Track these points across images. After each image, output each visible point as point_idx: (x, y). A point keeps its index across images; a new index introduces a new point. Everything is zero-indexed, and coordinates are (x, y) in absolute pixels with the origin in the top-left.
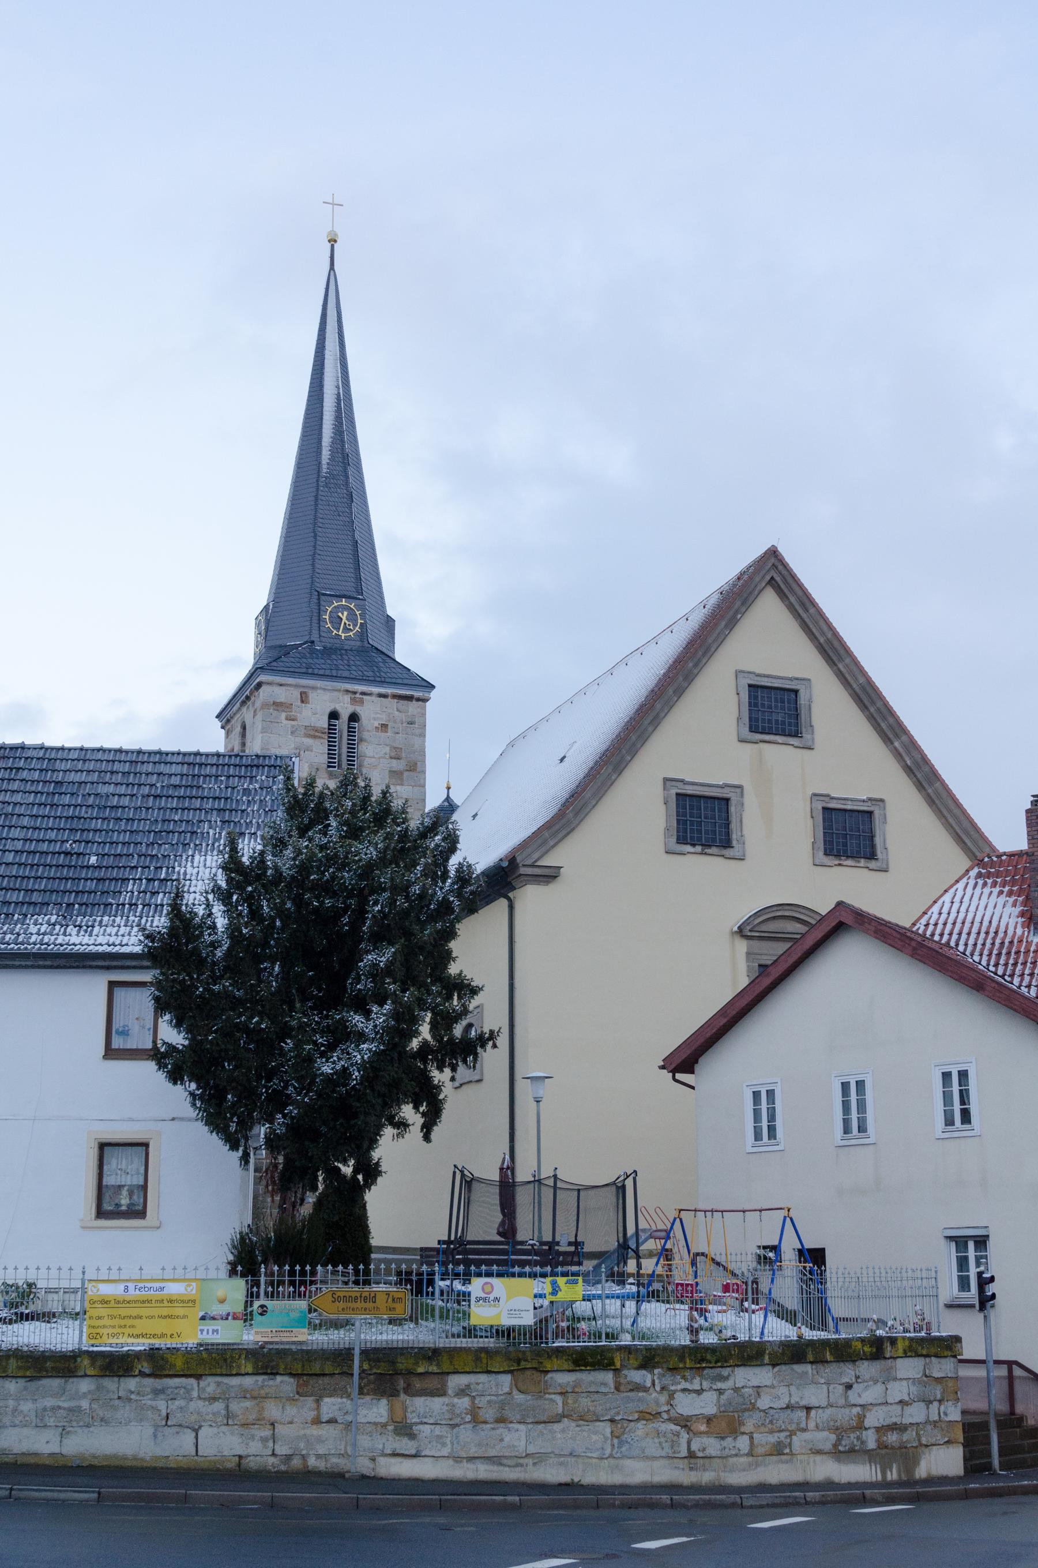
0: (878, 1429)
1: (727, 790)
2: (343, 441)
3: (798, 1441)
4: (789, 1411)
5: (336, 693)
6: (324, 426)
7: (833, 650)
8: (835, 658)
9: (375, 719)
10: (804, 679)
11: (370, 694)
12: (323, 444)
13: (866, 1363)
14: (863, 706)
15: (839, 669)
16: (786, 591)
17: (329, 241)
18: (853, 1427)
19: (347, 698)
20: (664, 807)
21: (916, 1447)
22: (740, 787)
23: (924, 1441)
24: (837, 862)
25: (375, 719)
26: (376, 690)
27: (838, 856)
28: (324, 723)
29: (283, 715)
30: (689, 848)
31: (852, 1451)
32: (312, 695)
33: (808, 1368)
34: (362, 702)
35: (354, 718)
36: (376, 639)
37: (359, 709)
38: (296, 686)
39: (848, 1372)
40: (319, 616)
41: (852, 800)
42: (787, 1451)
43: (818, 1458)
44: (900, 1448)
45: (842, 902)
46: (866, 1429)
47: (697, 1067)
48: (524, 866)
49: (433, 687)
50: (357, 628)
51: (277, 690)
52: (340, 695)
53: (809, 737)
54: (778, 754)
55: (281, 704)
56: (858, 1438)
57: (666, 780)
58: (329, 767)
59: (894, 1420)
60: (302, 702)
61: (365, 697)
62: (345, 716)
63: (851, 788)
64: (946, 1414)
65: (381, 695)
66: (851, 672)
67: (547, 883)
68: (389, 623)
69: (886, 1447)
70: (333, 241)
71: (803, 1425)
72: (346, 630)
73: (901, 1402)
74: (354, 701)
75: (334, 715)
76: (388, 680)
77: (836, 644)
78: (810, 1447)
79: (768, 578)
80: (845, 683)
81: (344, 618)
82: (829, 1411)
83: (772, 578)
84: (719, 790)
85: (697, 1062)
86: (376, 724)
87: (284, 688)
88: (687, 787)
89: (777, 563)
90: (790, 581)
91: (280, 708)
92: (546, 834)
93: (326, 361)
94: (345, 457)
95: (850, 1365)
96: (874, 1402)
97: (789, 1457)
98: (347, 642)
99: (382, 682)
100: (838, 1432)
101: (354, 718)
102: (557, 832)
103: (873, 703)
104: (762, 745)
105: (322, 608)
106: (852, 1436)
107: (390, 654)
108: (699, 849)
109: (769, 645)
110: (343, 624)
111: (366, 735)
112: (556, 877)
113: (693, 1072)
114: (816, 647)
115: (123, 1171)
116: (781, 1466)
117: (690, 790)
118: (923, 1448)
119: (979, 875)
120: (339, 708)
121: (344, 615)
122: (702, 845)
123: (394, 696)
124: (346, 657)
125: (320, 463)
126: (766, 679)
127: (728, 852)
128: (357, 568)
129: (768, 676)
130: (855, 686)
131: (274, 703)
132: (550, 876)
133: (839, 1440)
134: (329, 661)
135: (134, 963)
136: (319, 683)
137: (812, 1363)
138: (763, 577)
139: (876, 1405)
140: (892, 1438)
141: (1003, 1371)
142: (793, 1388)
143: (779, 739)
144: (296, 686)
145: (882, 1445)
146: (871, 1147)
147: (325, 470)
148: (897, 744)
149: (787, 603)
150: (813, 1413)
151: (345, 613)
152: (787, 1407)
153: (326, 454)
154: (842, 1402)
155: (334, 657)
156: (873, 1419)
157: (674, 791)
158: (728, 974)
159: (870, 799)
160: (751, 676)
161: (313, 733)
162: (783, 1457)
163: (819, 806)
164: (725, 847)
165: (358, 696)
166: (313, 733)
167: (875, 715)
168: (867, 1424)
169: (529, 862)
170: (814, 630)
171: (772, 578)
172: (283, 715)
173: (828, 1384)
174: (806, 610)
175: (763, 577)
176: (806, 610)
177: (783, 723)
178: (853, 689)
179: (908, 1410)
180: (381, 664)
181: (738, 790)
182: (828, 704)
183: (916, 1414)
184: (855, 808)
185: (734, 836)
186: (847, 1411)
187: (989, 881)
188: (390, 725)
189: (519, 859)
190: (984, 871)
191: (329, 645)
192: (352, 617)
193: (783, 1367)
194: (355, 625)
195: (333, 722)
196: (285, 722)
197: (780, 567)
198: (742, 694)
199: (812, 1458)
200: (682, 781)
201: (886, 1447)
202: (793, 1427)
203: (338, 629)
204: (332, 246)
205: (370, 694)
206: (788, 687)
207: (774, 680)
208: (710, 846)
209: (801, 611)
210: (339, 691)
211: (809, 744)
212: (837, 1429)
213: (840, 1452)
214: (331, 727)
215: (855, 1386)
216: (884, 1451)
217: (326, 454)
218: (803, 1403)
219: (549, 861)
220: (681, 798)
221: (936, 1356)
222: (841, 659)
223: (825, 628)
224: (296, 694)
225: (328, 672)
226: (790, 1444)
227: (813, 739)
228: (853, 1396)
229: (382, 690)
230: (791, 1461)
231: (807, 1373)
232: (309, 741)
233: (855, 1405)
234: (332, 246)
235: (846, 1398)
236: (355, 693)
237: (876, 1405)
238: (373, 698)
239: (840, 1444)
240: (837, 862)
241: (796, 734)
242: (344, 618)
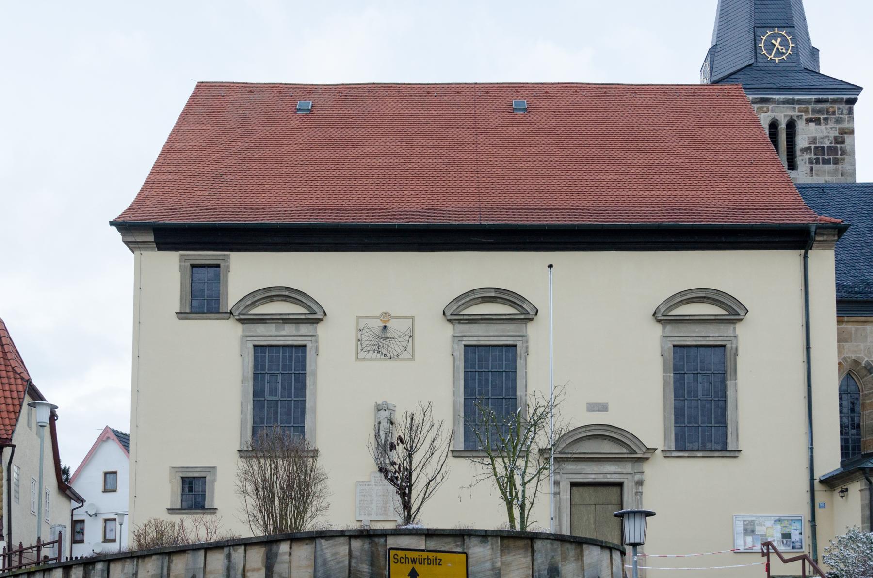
36: (805, 61)
40: (755, 44)
49: (861, 89)
62: (783, 126)
68: (814, 52)
81: (777, 44)
105: (757, 38)
110: (776, 48)
115: (749, 527)
135: (628, 435)
151: (779, 40)
158: (63, 464)
192: (784, 43)
194: (787, 50)
242: (777, 44)
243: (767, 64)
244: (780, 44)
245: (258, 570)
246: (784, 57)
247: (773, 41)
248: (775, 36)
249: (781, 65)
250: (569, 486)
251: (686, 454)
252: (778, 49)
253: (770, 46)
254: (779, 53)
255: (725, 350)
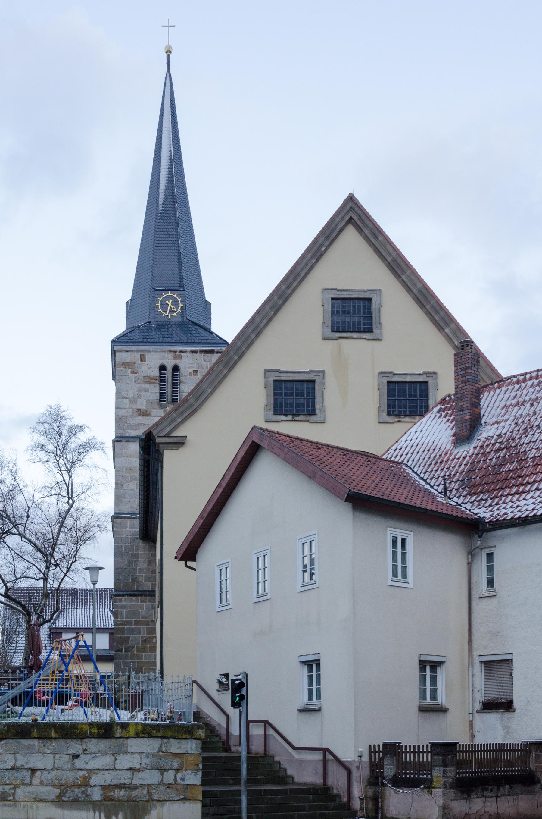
0: (104, 787)
1: (312, 375)
2: (173, 187)
3: (20, 793)
4: (14, 771)
5: (163, 353)
6: (161, 179)
7: (398, 265)
8: (399, 272)
9: (189, 368)
10: (375, 290)
11: (185, 352)
12: (160, 191)
13: (94, 741)
14: (421, 305)
15: (403, 280)
16: (361, 226)
17: (166, 52)
18: (79, 785)
19: (170, 356)
20: (264, 390)
21: (148, 801)
22: (323, 372)
23: (156, 797)
24: (397, 420)
25: (189, 368)
26: (189, 348)
27: (399, 415)
28: (156, 373)
29: (129, 370)
30: (283, 417)
31: (76, 801)
32: (148, 356)
33: (36, 742)
34: (180, 357)
35: (176, 368)
36: (194, 316)
37: (179, 362)
38: (137, 351)
39: (76, 746)
41: (410, 374)
42: (11, 798)
43: (41, 805)
44: (128, 801)
45: (255, 427)
46: (91, 786)
47: (198, 556)
48: (159, 437)
50: (179, 310)
51: (125, 355)
52: (166, 354)
53: (378, 331)
54: (354, 347)
55: (128, 364)
56: (83, 793)
57: (266, 371)
58: (160, 401)
59: (123, 781)
60: (141, 361)
61: (182, 354)
62: (169, 368)
63: (409, 367)
64: (183, 779)
65: (193, 352)
66: (411, 280)
67: (178, 448)
68: (207, 306)
69: (112, 800)
70: (169, 52)
71: (28, 781)
72: (171, 311)
73: (131, 769)
74: (175, 357)
75: (163, 368)
76: (196, 341)
77: (399, 261)
78: (33, 796)
79: (347, 218)
80: (409, 290)
81: (170, 304)
82: (54, 773)
83: (351, 218)
84: (306, 375)
85: (196, 553)
86: (190, 371)
87: (129, 353)
88: (282, 375)
89: (353, 206)
90: (364, 217)
91: (127, 366)
92: (174, 415)
93: (163, 135)
94: (174, 197)
95: (78, 742)
96: (101, 768)
97: (12, 803)
98: (172, 320)
99: (193, 343)
100: (62, 788)
101: (176, 368)
102: (182, 413)
103: (429, 302)
104: (341, 341)
106: (76, 791)
107: (207, 326)
108: (290, 417)
109: (352, 269)
111: (183, 379)
112: (183, 444)
113: (195, 561)
114: (386, 266)
116: (5, 808)
117: (284, 377)
118: (155, 803)
119: (440, 410)
120: (165, 362)
121: (169, 302)
122: (293, 415)
123: (202, 352)
124: (170, 329)
125: (158, 204)
126: (345, 293)
127: (312, 418)
128: (180, 270)
129: (347, 291)
130: (414, 291)
131: (123, 363)
132: (180, 443)
133: (63, 793)
134: (159, 333)
136: (151, 348)
137: (39, 738)
138: (343, 218)
139: (103, 770)
140: (121, 794)
141: (319, 756)
142: (18, 756)
143: (354, 335)
144: (137, 351)
145: (105, 798)
146: (269, 601)
147: (161, 209)
148: (447, 331)
149: (363, 235)
150: (38, 773)
152: (13, 768)
153: (162, 197)
154: (69, 766)
155: (163, 330)
156: (96, 780)
157: (272, 379)
159: (425, 373)
160: (333, 291)
161: (149, 380)
162: (6, 802)
163: (385, 381)
164: (310, 415)
165: (177, 353)
166: (149, 380)
167: (430, 310)
168: (92, 782)
169: (163, 434)
170: (383, 253)
171: (351, 218)
172: (129, 370)
173: (54, 753)
174: (377, 238)
175: (343, 218)
176: (377, 238)
177: (359, 323)
178: (414, 293)
179: (138, 775)
180: (194, 332)
181: (321, 374)
182: (395, 308)
183: (151, 777)
184: (414, 380)
185: (317, 407)
186: (73, 773)
187: (444, 414)
188: (199, 370)
189: (154, 433)
190: (443, 407)
191: (160, 323)
193: (10, 741)
194: (177, 308)
195: (163, 372)
196: (130, 375)
197: (356, 209)
198: (326, 306)
199: (35, 804)
200: (278, 371)
201: (112, 800)
202: (18, 782)
203: (166, 312)
204: (169, 56)
205: (185, 352)
206: (363, 297)
207: (351, 293)
208: (298, 415)
209: (373, 240)
210: (165, 351)
211: (379, 337)
212: (61, 785)
213: (63, 801)
214: (162, 376)
215: (82, 756)
216: (109, 803)
217: (162, 197)
218: (30, 766)
219: (179, 433)
220: (278, 383)
221: (174, 738)
222: (404, 272)
223: (391, 250)
224: (138, 356)
225: (156, 340)
226: (14, 794)
227: (381, 333)
228: (78, 763)
229: (193, 348)
230: (15, 805)
231: (34, 745)
232: (147, 386)
233: (82, 770)
234: (169, 56)
235: (73, 764)
236: (175, 352)
237: (103, 770)
238: (188, 354)
239: (64, 796)
240: (397, 420)
241: (369, 330)
242: (170, 304)
243: (162, 320)
244: (172, 304)
245: (132, 456)
246: (175, 314)
247: (167, 302)
248: (168, 298)
249: (172, 320)
250: (516, 705)
251: (160, 474)
252: (171, 307)
253: (164, 306)
254: (171, 311)
255: (238, 746)
